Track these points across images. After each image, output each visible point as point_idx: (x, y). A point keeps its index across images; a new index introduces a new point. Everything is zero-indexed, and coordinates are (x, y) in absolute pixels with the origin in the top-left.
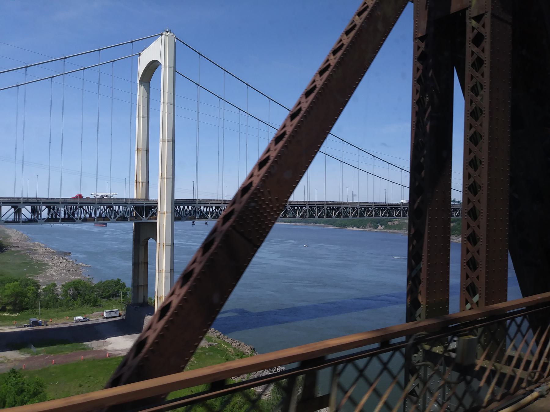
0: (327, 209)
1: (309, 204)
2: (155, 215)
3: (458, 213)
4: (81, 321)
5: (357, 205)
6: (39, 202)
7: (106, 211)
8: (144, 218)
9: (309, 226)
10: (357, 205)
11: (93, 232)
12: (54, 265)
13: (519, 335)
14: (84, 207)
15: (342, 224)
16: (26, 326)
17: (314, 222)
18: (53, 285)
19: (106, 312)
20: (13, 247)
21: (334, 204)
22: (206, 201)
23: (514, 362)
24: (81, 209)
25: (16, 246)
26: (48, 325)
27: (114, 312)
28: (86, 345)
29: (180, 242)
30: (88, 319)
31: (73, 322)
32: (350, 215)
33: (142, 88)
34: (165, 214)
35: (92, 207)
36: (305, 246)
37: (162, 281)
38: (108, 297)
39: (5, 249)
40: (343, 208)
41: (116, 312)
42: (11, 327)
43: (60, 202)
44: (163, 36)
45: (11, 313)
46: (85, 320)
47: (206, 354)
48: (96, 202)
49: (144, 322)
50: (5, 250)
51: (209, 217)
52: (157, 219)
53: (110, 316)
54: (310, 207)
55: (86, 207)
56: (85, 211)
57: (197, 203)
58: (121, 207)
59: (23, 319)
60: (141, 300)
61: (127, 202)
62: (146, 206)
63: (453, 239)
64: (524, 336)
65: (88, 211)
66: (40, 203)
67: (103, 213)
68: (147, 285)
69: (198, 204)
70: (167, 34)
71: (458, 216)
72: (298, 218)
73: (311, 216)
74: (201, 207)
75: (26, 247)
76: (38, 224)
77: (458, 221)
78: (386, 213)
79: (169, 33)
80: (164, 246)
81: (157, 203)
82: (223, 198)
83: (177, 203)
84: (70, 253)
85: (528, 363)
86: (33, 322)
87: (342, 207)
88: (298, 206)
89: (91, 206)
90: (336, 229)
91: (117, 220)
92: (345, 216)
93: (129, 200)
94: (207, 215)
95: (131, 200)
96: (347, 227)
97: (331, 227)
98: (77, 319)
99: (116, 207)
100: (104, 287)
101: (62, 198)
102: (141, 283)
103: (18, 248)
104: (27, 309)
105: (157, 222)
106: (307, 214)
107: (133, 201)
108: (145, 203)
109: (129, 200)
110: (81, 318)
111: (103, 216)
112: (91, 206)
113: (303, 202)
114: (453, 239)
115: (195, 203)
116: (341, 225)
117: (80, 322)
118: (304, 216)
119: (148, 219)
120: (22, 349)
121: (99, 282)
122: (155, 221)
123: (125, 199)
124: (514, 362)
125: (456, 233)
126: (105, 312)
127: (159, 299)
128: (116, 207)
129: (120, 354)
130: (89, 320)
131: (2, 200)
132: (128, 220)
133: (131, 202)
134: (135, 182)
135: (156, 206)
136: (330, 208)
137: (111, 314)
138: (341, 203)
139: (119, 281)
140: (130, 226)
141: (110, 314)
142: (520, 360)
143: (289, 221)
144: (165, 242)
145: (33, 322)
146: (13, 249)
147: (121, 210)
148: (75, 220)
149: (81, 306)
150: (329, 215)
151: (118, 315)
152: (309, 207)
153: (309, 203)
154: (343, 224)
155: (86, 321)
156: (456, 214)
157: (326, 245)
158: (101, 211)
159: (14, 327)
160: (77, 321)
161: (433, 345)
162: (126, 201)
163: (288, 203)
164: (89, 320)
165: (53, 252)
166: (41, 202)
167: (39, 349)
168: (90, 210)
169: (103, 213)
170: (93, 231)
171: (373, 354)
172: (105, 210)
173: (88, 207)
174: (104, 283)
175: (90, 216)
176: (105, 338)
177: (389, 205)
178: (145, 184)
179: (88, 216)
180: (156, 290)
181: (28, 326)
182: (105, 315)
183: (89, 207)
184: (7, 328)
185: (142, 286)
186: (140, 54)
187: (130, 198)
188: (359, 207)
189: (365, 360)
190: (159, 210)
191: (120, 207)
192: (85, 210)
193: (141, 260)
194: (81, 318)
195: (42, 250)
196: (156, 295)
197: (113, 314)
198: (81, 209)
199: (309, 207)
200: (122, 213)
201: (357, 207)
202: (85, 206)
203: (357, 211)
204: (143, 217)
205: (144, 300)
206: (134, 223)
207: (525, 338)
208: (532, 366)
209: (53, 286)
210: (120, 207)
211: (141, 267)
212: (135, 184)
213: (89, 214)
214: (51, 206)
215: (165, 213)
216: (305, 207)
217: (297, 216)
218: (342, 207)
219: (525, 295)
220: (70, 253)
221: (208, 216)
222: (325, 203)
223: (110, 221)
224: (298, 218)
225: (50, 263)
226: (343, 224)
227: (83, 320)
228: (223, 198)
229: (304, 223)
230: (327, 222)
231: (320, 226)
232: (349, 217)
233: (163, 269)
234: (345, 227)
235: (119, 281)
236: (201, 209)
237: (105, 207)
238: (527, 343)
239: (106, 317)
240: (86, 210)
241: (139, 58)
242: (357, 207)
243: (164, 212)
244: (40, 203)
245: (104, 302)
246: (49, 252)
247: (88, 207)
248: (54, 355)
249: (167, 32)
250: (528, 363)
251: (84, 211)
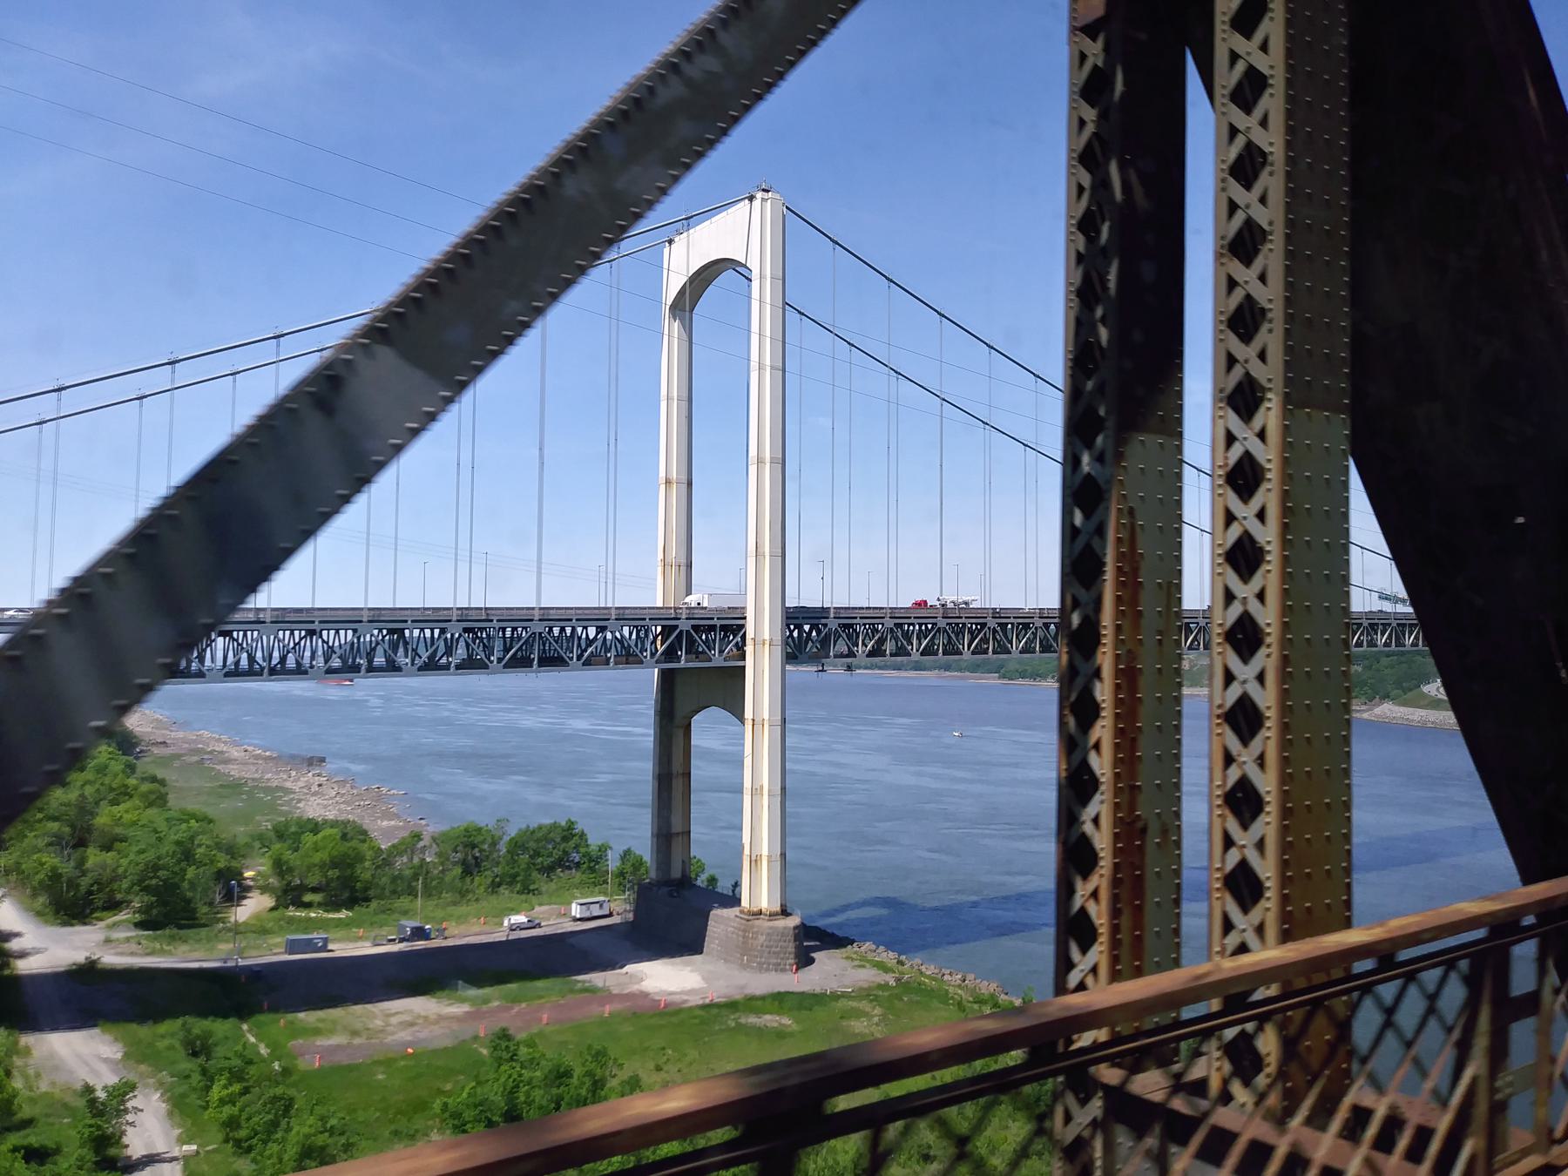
0: (945, 631)
1: (837, 616)
2: (741, 647)
3: (1414, 638)
4: (522, 927)
5: (1033, 617)
6: (490, 618)
7: (297, 647)
8: (495, 662)
9: (930, 677)
10: (1033, 617)
11: (329, 700)
12: (305, 791)
13: (1390, 1039)
14: (235, 634)
15: (1026, 670)
16: (394, 940)
17: (940, 668)
18: (415, 836)
19: (581, 905)
20: (153, 744)
21: (805, 615)
22: (655, 611)
23: (1372, 1131)
24: (227, 638)
25: (161, 743)
26: (446, 938)
27: (598, 905)
28: (584, 982)
29: (592, 725)
30: (537, 922)
31: (501, 929)
32: (915, 650)
33: (676, 324)
34: (767, 646)
35: (256, 633)
36: (956, 734)
37: (760, 818)
38: (549, 870)
39: (138, 750)
40: (891, 629)
41: (601, 904)
42: (359, 944)
43: (365, 619)
44: (757, 203)
45: (327, 911)
46: (530, 925)
47: (903, 1000)
48: (267, 621)
49: (707, 925)
50: (139, 753)
51: (646, 657)
52: (743, 658)
53: (587, 914)
54: (899, 626)
55: (288, 633)
56: (238, 644)
57: (832, 616)
58: (343, 631)
59: (372, 924)
60: (676, 873)
61: (679, 616)
62: (721, 625)
63: (1358, 711)
64: (1409, 1045)
65: (245, 645)
66: (492, 621)
67: (288, 652)
68: (690, 832)
69: (687, 619)
70: (766, 195)
71: (1386, 644)
72: (916, 656)
73: (901, 651)
74: (624, 628)
75: (187, 746)
76: (204, 683)
77: (1368, 659)
78: (985, 640)
79: (770, 193)
80: (766, 726)
81: (745, 618)
82: (832, 603)
83: (794, 617)
84: (322, 760)
85: (1423, 1135)
86: (412, 929)
87: (992, 623)
88: (916, 621)
89: (252, 631)
90: (1023, 687)
91: (505, 667)
92: (999, 649)
93: (268, 615)
94: (640, 652)
95: (618, 611)
96: (1040, 681)
97: (992, 680)
98: (512, 922)
99: (328, 633)
100: (538, 841)
101: (370, 609)
102: (677, 826)
103: (165, 749)
104: (367, 900)
105: (744, 668)
106: (889, 646)
107: (656, 615)
108: (718, 619)
109: (363, 613)
110: (521, 919)
111: (291, 662)
112: (252, 631)
113: (1054, 611)
114: (1358, 711)
115: (827, 618)
116: (1023, 675)
117: (521, 929)
118: (876, 652)
119: (725, 660)
120: (439, 994)
121: (520, 830)
122: (740, 663)
123: (486, 609)
124: (1372, 1131)
125: (1363, 694)
126: (574, 905)
127: (753, 863)
128: (328, 633)
129: (686, 1001)
130: (539, 925)
131: (412, 616)
132: (611, 665)
133: (370, 619)
134: (660, 564)
135: (743, 626)
136: (923, 627)
137: (591, 909)
138: (986, 611)
139: (571, 825)
140: (652, 675)
141: (589, 909)
142: (1393, 1123)
143: (869, 665)
144: (766, 716)
145: (412, 929)
146: (156, 750)
147: (343, 642)
148: (567, 662)
149: (493, 892)
150: (952, 650)
151: (608, 913)
152: (689, 628)
153: (839, 613)
154: (1029, 671)
155: (534, 928)
156: (1409, 638)
157: (1005, 731)
158: (284, 647)
159: (368, 944)
160: (514, 927)
161: (1135, 1069)
162: (488, 614)
163: (832, 616)
164: (539, 924)
165: (270, 758)
166: (495, 618)
167: (487, 991)
168: (249, 641)
169: (377, 644)
170: (329, 698)
171: (1001, 1084)
172: (295, 644)
173: (245, 635)
174: (533, 832)
175: (252, 659)
176: (618, 966)
177: (996, 613)
178: (683, 569)
179: (244, 662)
180: (744, 841)
181: (402, 940)
182: (576, 910)
183: (249, 633)
184: (351, 945)
185: (678, 834)
186: (670, 242)
187: (369, 606)
188: (1039, 623)
189: (970, 1109)
190: (750, 635)
191: (340, 631)
192: (237, 640)
193: (677, 767)
194: (521, 919)
195: (235, 753)
196: (747, 851)
197: (596, 911)
198: (227, 638)
199: (689, 628)
200: (346, 650)
201: (1033, 624)
202: (238, 631)
203: (1034, 634)
204: (492, 658)
205: (684, 871)
206: (656, 670)
207: (1413, 1052)
208: (1434, 1147)
209: (416, 839)
210: (340, 631)
211: (677, 784)
212: (660, 569)
213: (247, 652)
214: (902, 624)
215: (767, 643)
216: (883, 624)
217: (858, 651)
218: (992, 623)
219: (1528, 878)
220: (322, 760)
221: (645, 654)
222: (455, 612)
223: (488, 669)
224: (916, 656)
225: (288, 785)
226: (1029, 671)
227: (529, 926)
228: (832, 603)
229: (911, 669)
230: (978, 666)
231: (958, 677)
232: (855, 656)
233: (762, 787)
234: (1035, 679)
235: (571, 825)
236: (624, 632)
237: (385, 632)
238: (1422, 1071)
239: (578, 916)
240: (240, 641)
241: (666, 251)
242: (1033, 624)
243: (764, 640)
244: (492, 621)
245: (540, 881)
246: (257, 757)
247: (245, 635)
248: (528, 1005)
249: (768, 191)
250: (1423, 1135)
251: (235, 644)
